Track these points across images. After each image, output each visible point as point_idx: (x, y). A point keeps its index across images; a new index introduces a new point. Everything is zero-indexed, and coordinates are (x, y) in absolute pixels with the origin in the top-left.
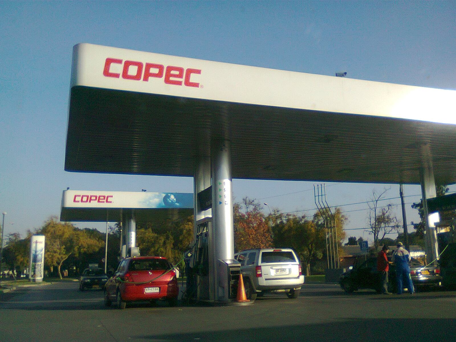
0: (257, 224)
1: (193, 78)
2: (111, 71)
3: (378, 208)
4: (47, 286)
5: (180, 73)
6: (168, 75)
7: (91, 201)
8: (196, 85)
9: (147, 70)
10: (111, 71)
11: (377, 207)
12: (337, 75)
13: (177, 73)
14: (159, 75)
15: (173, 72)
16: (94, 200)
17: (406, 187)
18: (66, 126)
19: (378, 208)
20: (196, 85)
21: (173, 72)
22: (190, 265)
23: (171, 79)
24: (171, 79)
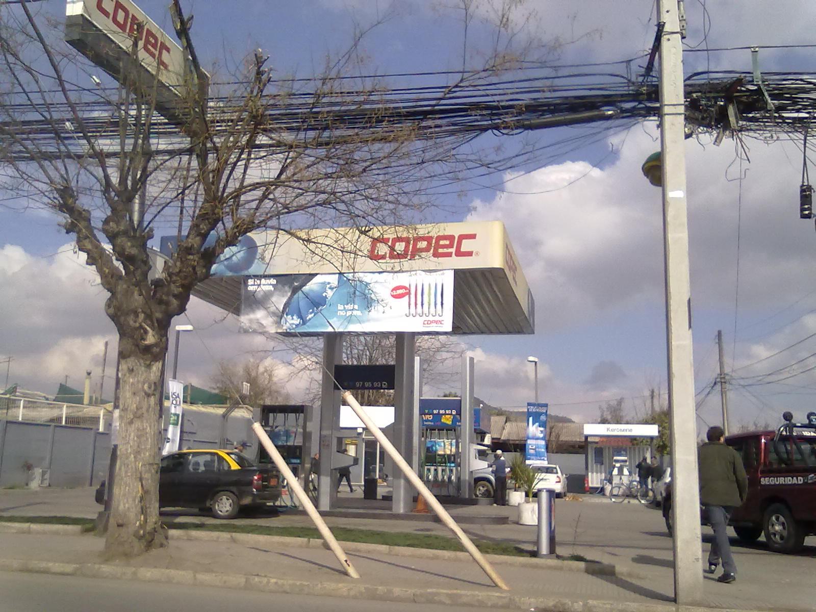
0: (178, 115)
1: (466, 246)
3: (361, 73)
4: (592, 457)
5: (450, 243)
8: (469, 254)
9: (415, 245)
11: (359, 75)
12: (689, 299)
13: (447, 242)
14: (427, 250)
15: (442, 242)
17: (249, 284)
18: (671, 275)
19: (361, 73)
20: (469, 254)
21: (442, 242)
22: (227, 249)
23: (440, 251)
24: (440, 251)
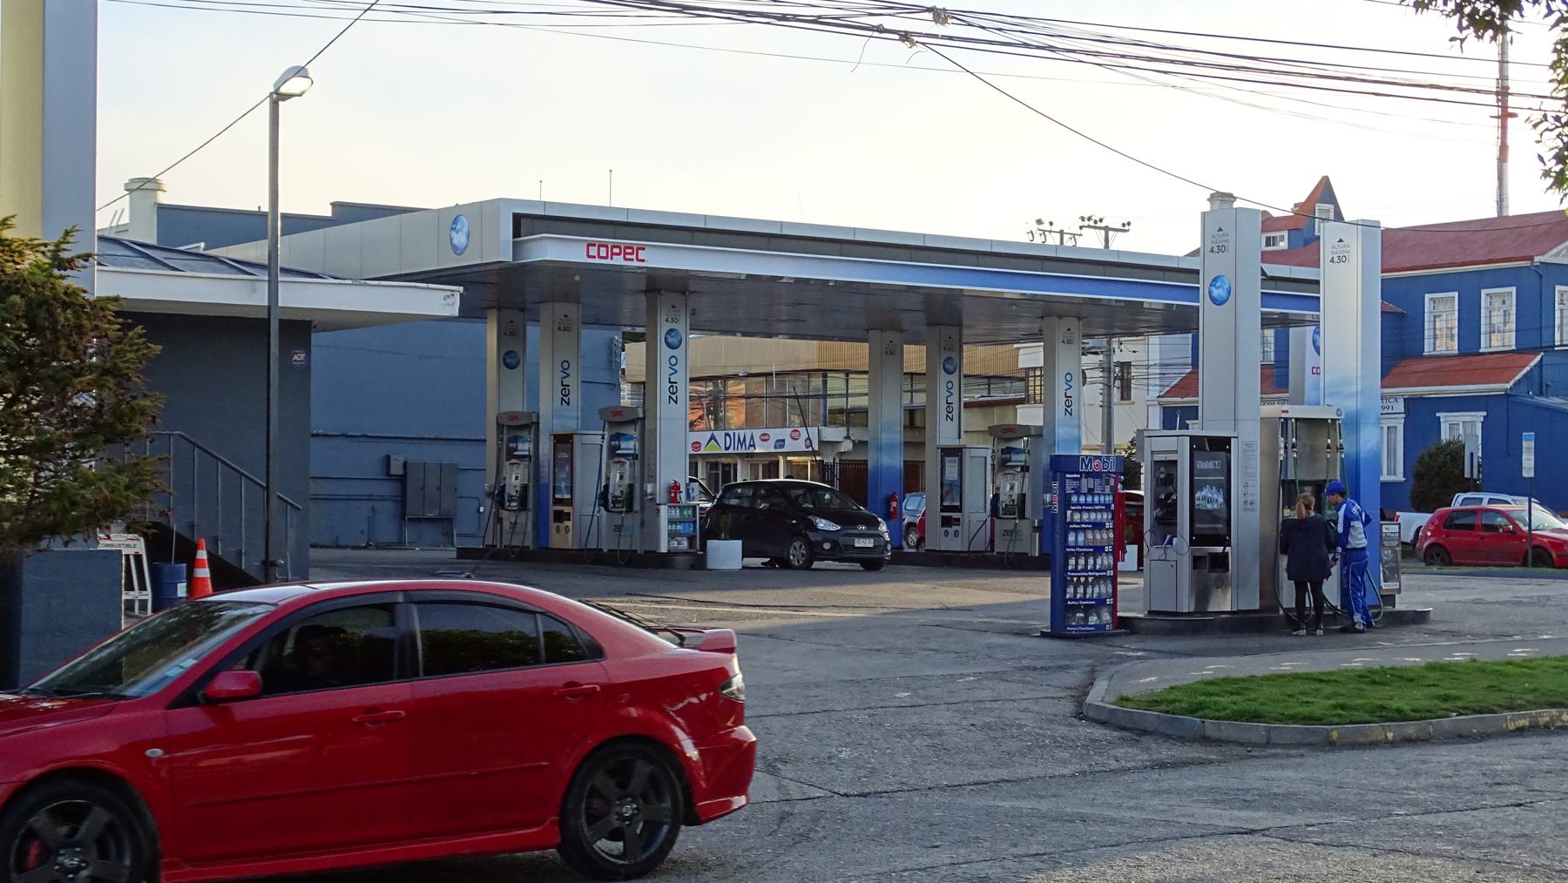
2: (601, 255)
6: (625, 253)
7: (614, 256)
10: (591, 254)
13: (630, 251)
14: (619, 254)
16: (617, 254)
23: (627, 256)
24: (627, 256)
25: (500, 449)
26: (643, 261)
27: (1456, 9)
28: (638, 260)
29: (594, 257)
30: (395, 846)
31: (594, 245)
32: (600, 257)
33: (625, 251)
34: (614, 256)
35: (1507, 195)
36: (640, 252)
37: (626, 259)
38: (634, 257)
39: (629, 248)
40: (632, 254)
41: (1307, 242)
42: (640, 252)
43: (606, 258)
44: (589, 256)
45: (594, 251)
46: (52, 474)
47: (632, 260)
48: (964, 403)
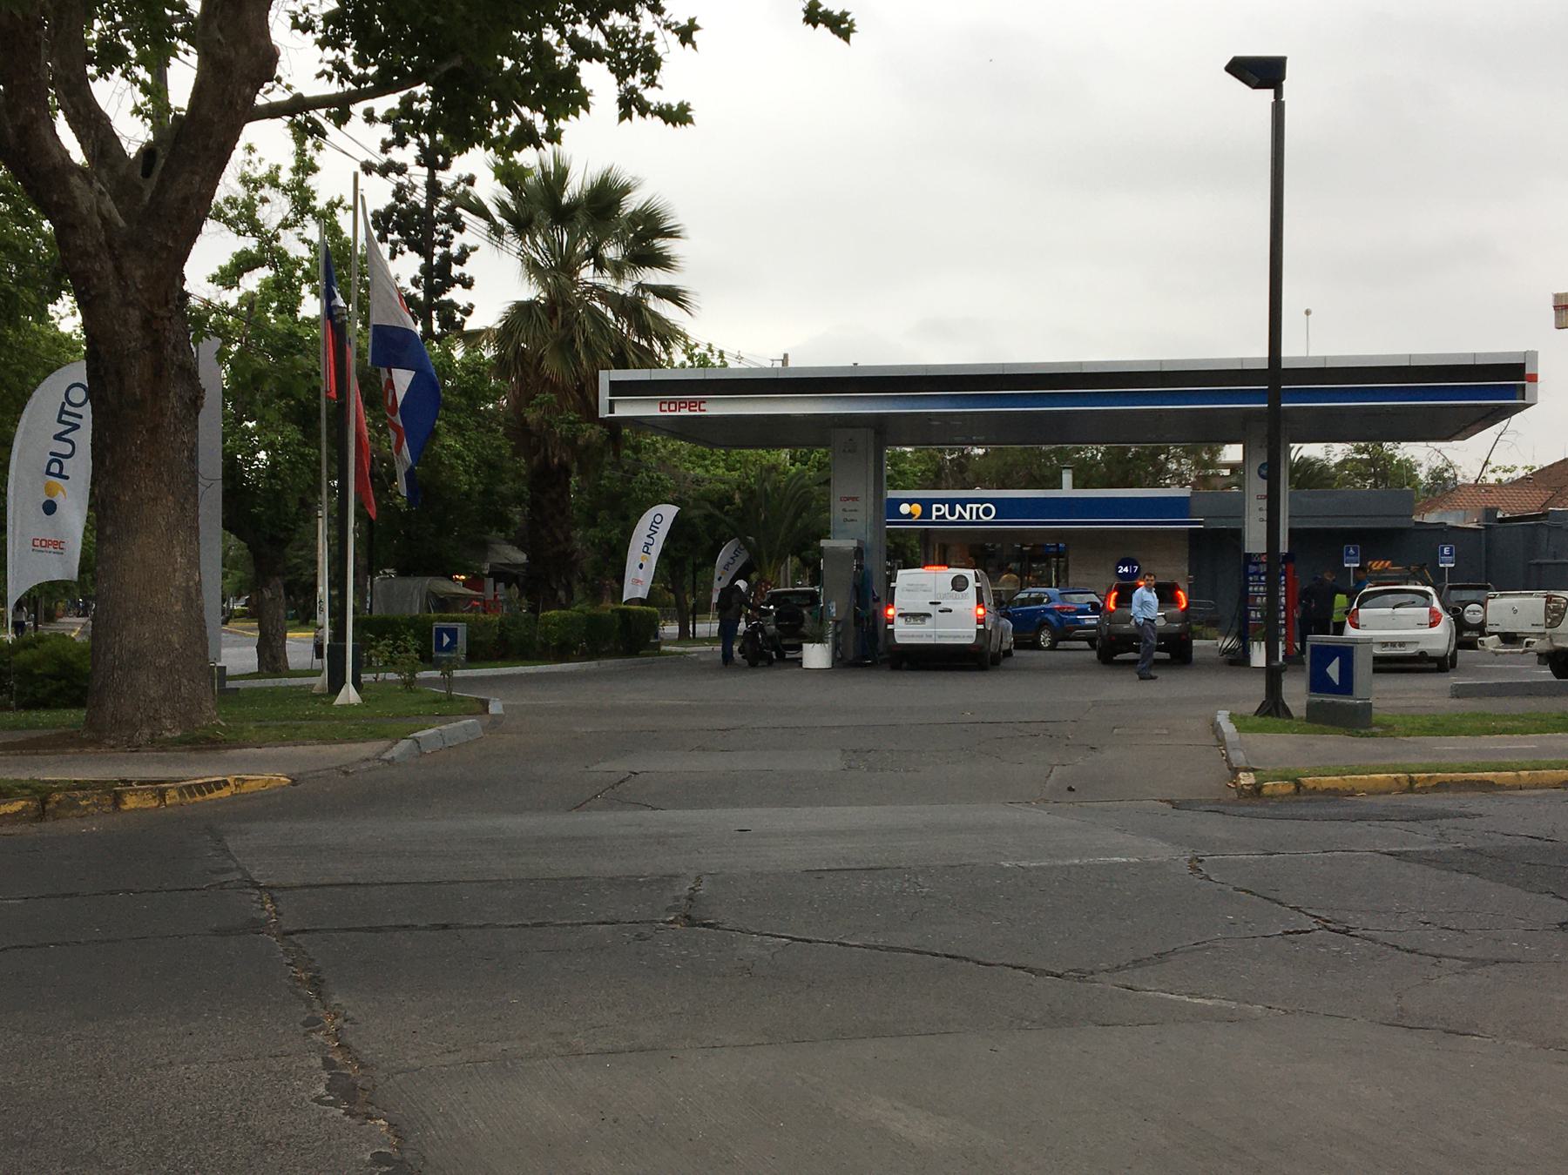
6: (690, 407)
10: (663, 409)
14: (685, 407)
23: (692, 408)
24: (692, 408)
25: (922, 636)
26: (704, 410)
27: (312, 163)
28: (700, 410)
29: (665, 411)
30: (1510, 663)
31: (665, 403)
32: (670, 411)
33: (690, 404)
34: (64, 473)
35: (780, 668)
36: (702, 405)
37: (690, 410)
38: (697, 408)
39: (683, 403)
40: (696, 406)
41: (944, 549)
42: (702, 405)
43: (675, 411)
44: (661, 411)
45: (665, 407)
46: (269, 922)
47: (696, 411)
48: (1313, 647)
